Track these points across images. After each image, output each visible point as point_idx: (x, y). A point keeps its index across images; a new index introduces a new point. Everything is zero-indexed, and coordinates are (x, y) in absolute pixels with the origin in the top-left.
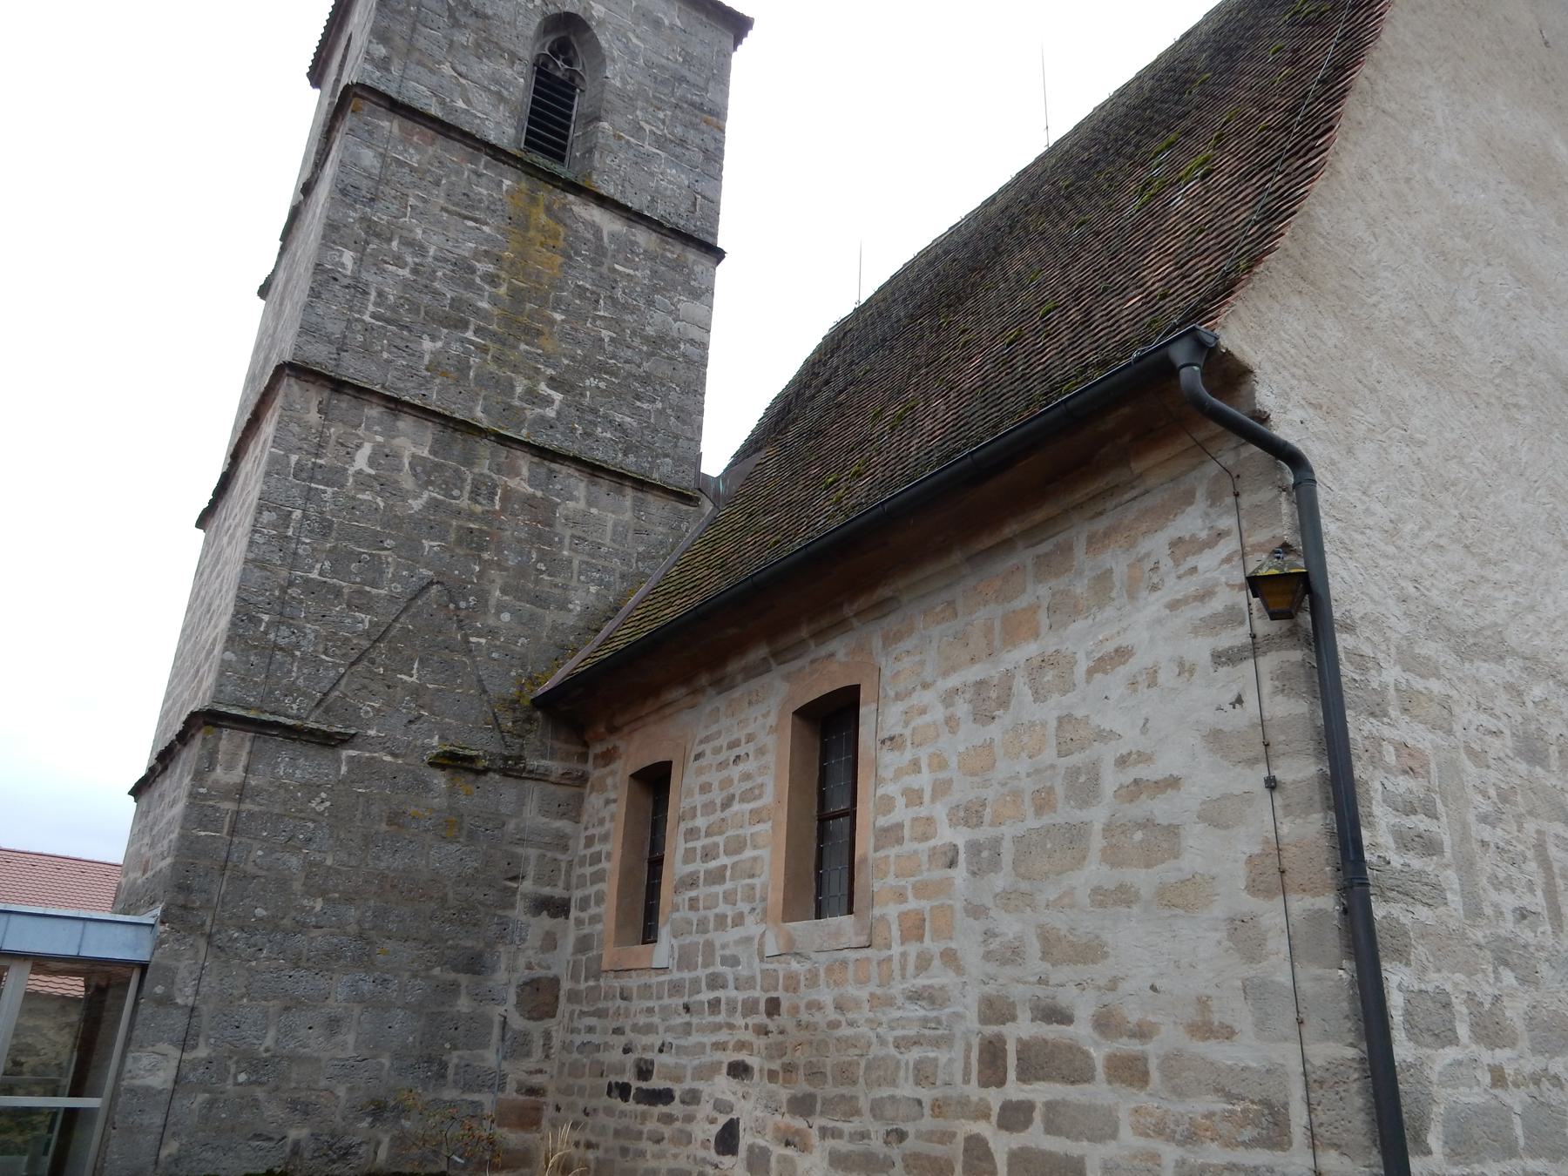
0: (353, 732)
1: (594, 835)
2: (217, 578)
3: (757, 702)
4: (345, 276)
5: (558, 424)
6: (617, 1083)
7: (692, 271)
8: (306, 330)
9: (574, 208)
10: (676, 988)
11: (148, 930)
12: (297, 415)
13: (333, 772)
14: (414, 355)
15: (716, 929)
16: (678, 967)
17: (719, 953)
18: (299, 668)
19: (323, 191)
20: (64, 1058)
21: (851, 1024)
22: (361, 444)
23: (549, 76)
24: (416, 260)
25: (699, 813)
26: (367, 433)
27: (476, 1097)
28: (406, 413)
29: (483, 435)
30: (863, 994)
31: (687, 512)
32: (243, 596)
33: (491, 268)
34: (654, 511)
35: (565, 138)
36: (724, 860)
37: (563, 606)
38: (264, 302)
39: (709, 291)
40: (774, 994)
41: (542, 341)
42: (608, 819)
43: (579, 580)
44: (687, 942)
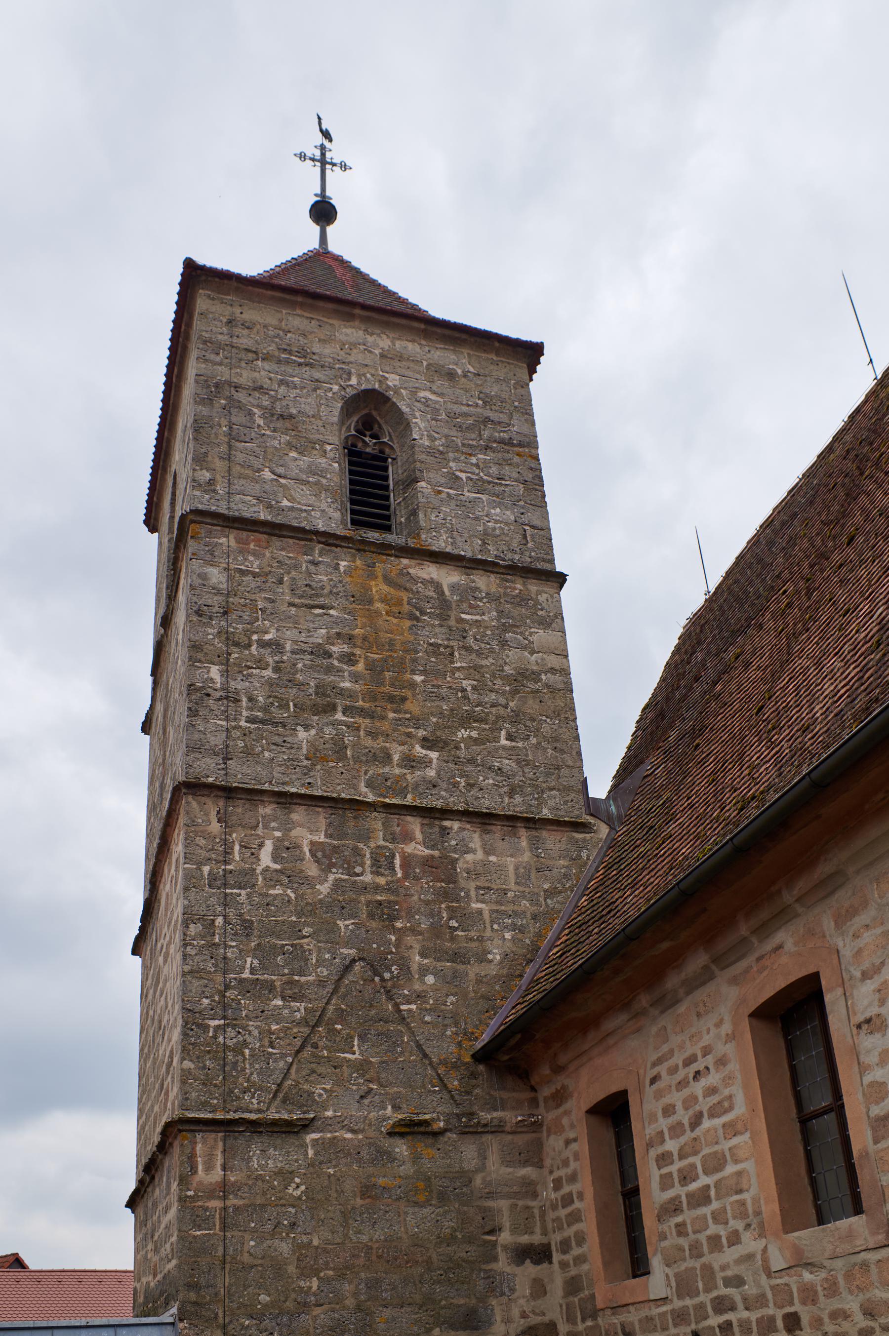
0: (312, 1116)
2: (161, 996)
3: (707, 1012)
4: (216, 690)
7: (537, 602)
8: (193, 748)
9: (411, 571)
11: (170, 1328)
12: (201, 828)
13: (302, 1157)
14: (292, 748)
15: (711, 1252)
16: (678, 1296)
17: (720, 1275)
18: (251, 1064)
19: (180, 618)
22: (263, 842)
23: (359, 454)
24: (276, 658)
25: (667, 1136)
26: (266, 831)
28: (296, 804)
29: (373, 809)
31: (584, 840)
33: (345, 648)
34: (551, 846)
35: (387, 508)
36: (704, 1180)
37: (482, 958)
38: (148, 737)
39: (559, 616)
40: (791, 1310)
41: (408, 705)
42: (571, 1159)
43: (492, 929)
44: (683, 1268)
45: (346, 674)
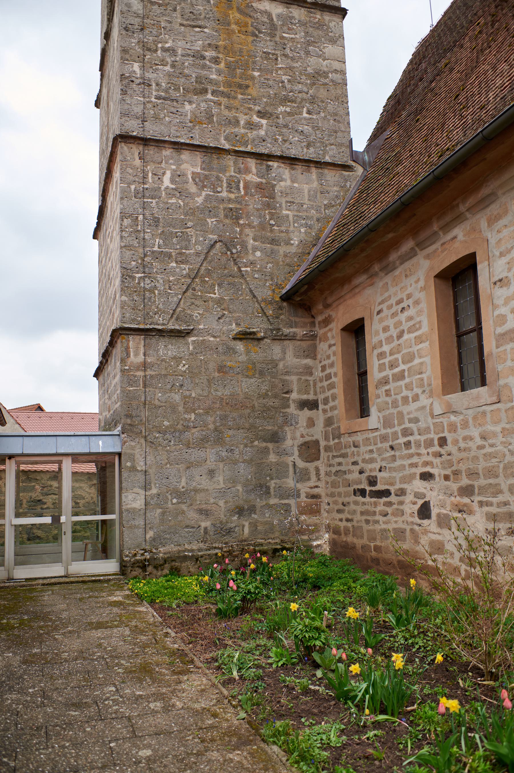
0: (192, 328)
1: (325, 365)
3: (411, 275)
5: (267, 138)
6: (358, 489)
7: (329, 27)
8: (124, 114)
10: (384, 438)
11: (117, 437)
12: (130, 163)
14: (182, 115)
15: (403, 405)
17: (406, 417)
20: (95, 499)
21: (492, 446)
22: (165, 172)
24: (173, 59)
25: (384, 343)
27: (286, 501)
28: (184, 149)
30: (498, 429)
32: (124, 266)
33: (214, 54)
34: (329, 179)
36: (402, 367)
37: (288, 243)
39: (341, 36)
41: (250, 90)
42: (332, 355)
43: (294, 226)
44: (387, 413)
45: (214, 70)
